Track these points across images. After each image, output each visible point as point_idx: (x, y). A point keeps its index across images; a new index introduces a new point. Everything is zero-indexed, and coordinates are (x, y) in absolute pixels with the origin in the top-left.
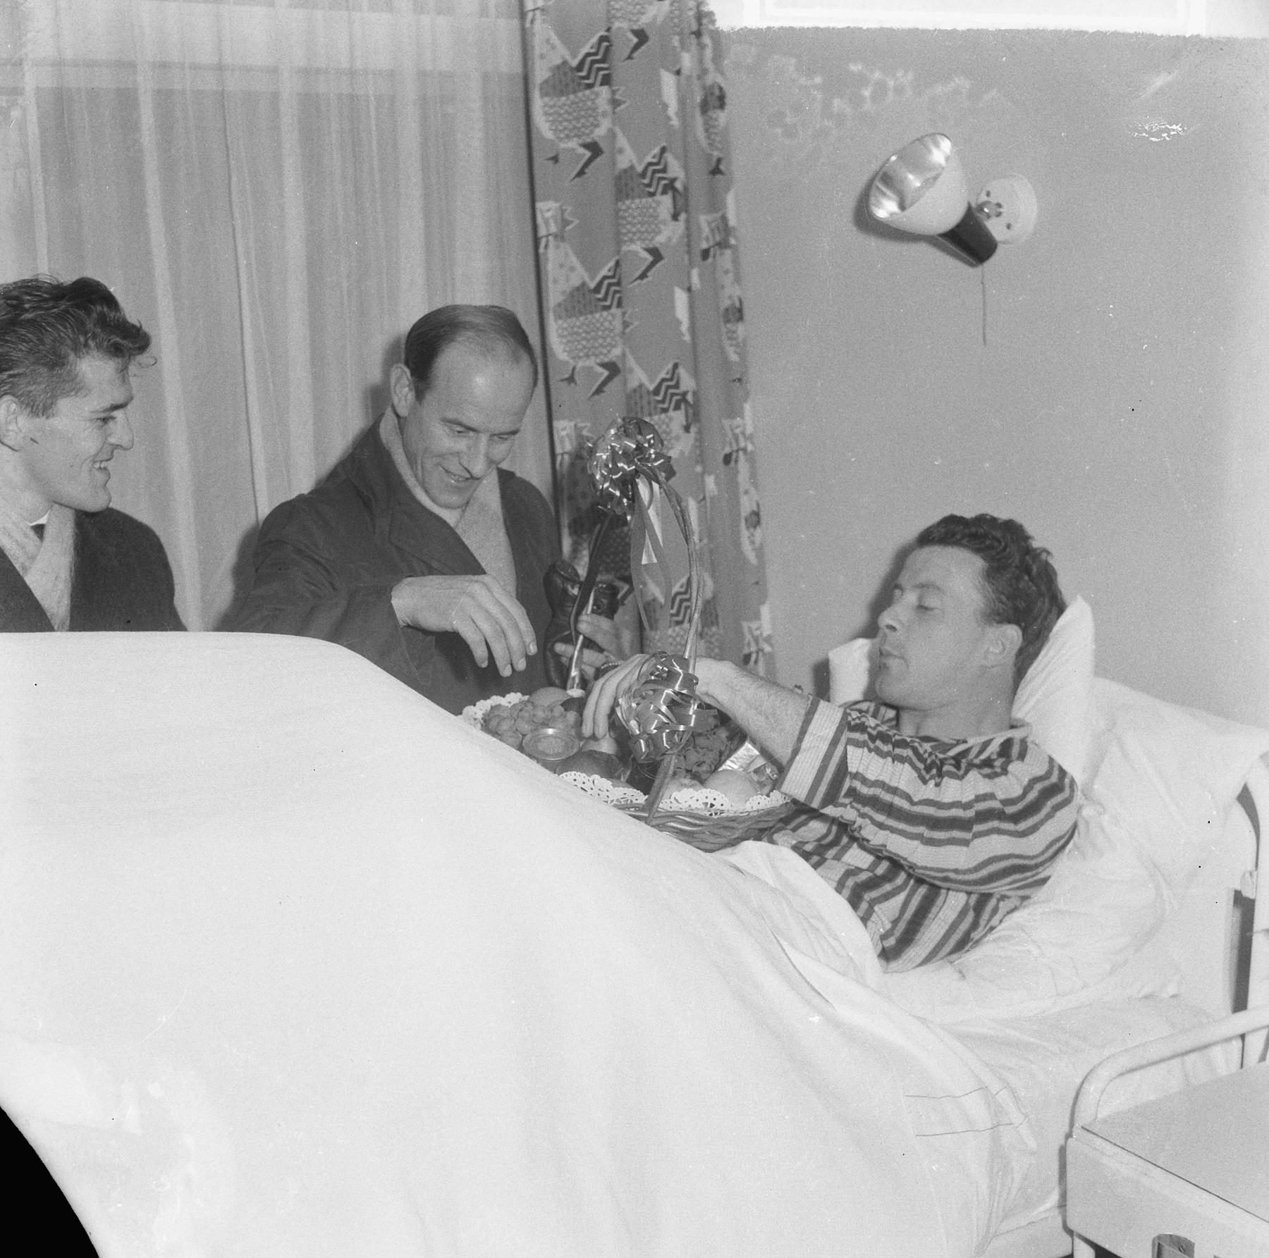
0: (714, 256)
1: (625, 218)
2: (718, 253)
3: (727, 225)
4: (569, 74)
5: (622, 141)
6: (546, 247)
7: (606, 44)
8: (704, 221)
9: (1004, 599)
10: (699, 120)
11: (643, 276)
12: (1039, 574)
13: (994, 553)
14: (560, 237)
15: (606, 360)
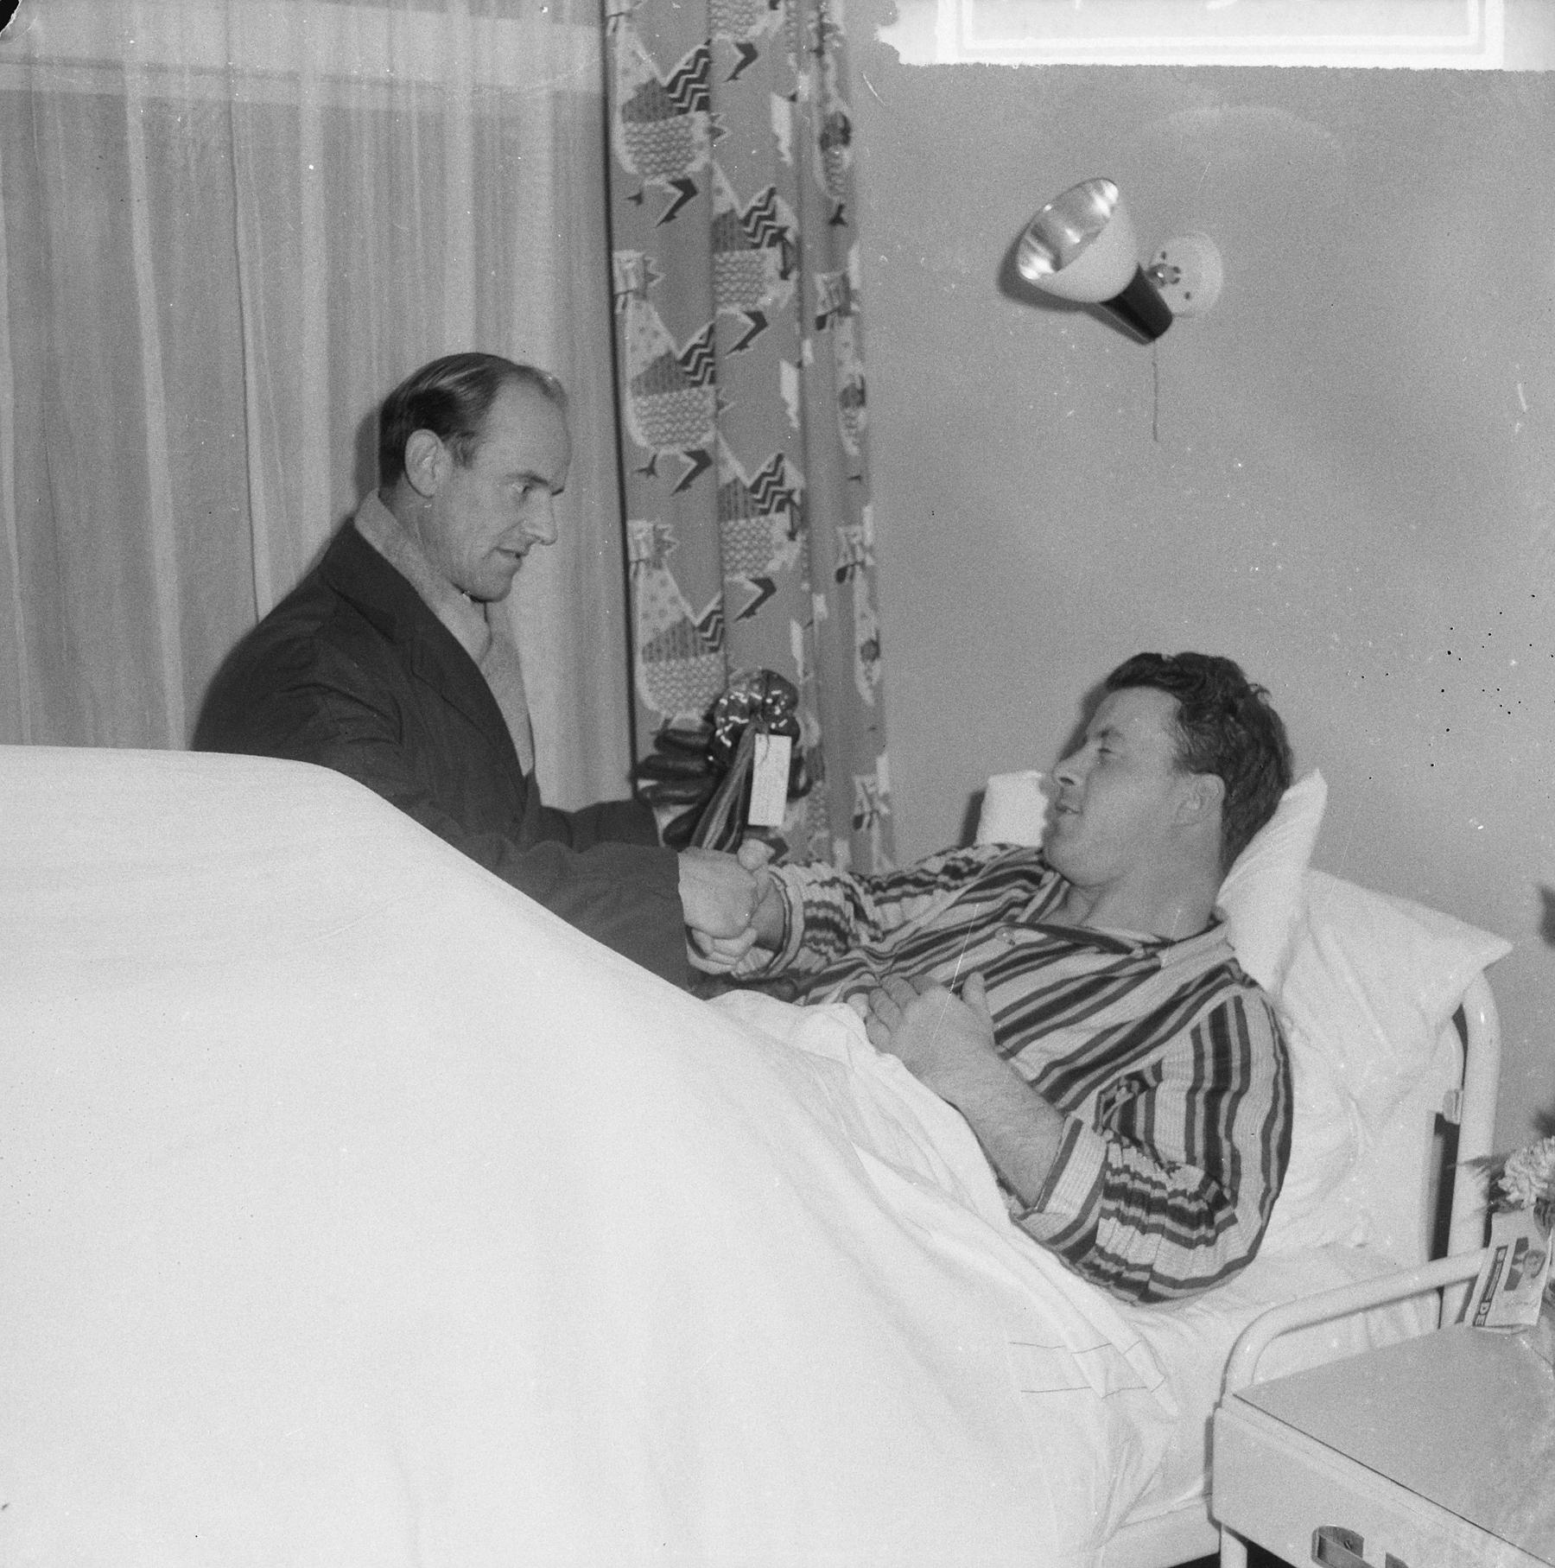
1: (722, 274)
3: (848, 288)
6: (624, 306)
10: (818, 156)
11: (742, 346)
14: (642, 294)
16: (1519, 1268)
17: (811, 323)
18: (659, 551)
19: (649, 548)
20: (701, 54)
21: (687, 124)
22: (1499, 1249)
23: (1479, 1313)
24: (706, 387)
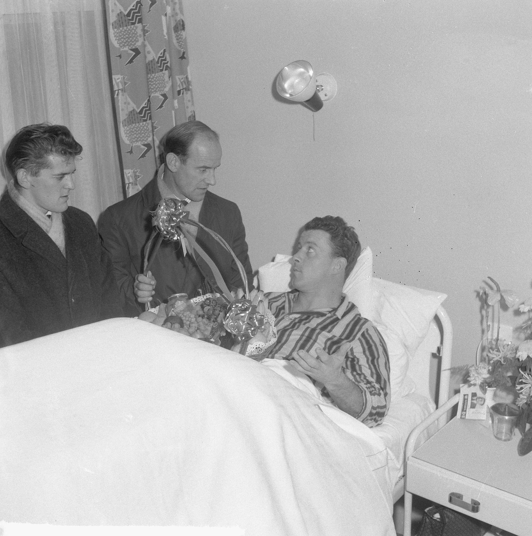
0: (183, 94)
2: (185, 92)
3: (188, 80)
4: (123, 18)
5: (149, 48)
6: (118, 95)
7: (139, 5)
8: (179, 79)
9: (339, 248)
10: (174, 35)
11: (161, 107)
12: (351, 237)
13: (333, 231)
14: (123, 90)
15: (146, 143)
16: (475, 402)
17: (176, 93)
18: (136, 179)
19: (132, 179)
20: (138, 3)
21: (135, 28)
22: (465, 395)
23: (462, 415)
24: (148, 121)
